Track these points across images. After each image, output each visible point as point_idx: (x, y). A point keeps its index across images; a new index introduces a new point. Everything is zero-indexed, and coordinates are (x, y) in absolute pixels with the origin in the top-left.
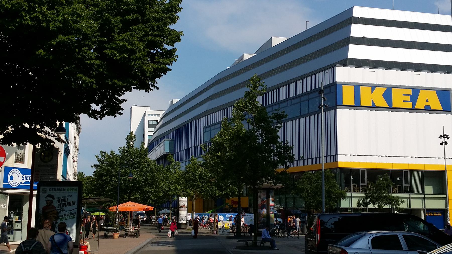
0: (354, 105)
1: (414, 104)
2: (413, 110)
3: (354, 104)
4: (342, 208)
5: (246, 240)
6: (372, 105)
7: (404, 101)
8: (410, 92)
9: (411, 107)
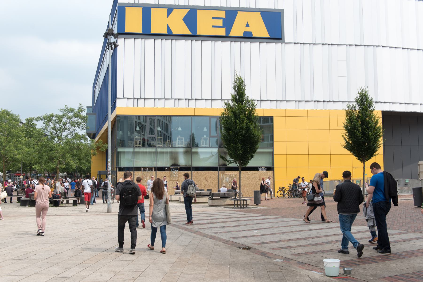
1: (228, 30)
2: (227, 37)
7: (213, 26)
8: (223, 14)
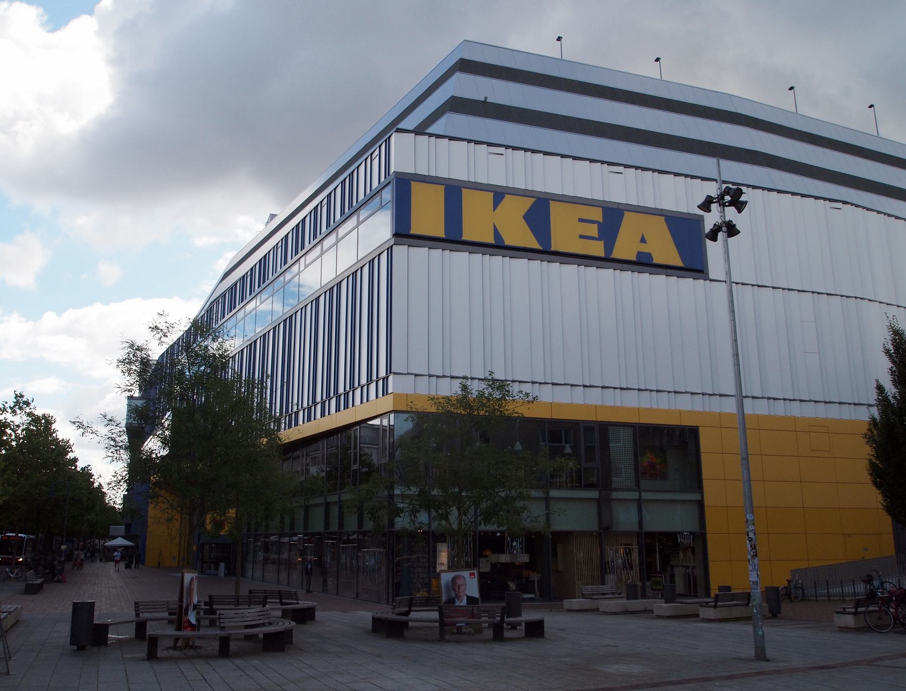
0: (494, 243)
1: (609, 247)
2: (608, 261)
3: (442, 235)
4: (110, 536)
5: (506, 543)
6: (445, 235)
9: (602, 254)
